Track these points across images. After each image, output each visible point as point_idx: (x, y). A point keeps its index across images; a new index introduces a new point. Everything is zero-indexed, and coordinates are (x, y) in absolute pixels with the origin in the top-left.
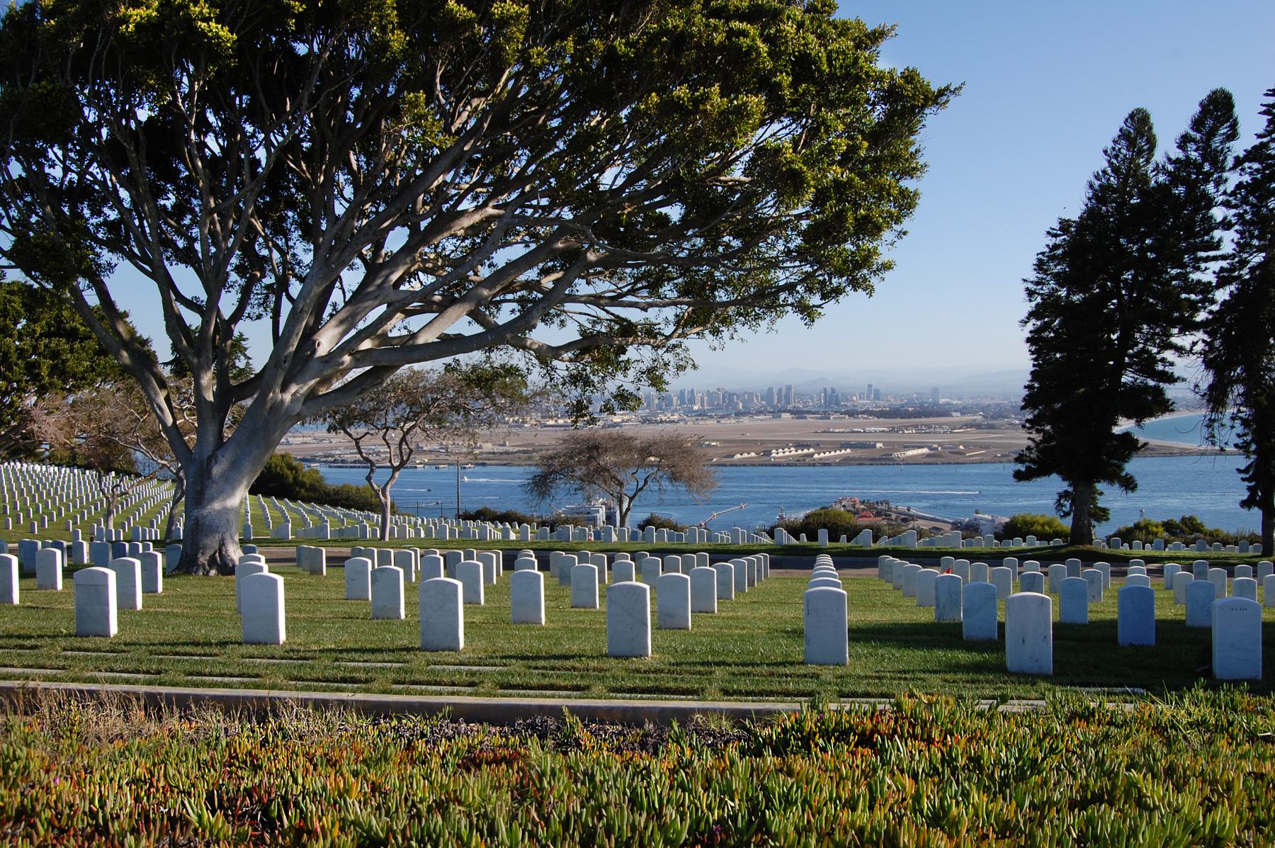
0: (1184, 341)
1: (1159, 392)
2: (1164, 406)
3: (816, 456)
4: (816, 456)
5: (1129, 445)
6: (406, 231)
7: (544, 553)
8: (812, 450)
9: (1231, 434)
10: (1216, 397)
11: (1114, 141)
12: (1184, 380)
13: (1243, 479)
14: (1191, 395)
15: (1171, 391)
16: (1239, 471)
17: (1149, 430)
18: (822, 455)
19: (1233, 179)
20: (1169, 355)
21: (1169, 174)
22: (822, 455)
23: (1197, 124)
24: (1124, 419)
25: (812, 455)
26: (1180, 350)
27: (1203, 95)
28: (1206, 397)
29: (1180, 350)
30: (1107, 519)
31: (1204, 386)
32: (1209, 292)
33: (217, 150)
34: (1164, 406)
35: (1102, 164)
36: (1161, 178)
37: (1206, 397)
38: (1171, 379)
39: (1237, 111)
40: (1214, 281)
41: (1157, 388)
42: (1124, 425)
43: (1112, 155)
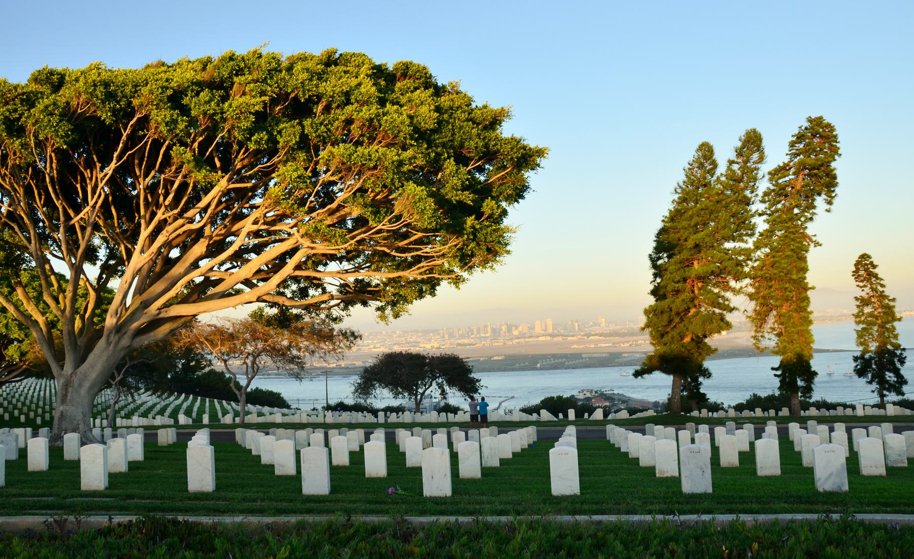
1: (722, 319)
3: (567, 363)
4: (567, 363)
7: (391, 430)
8: (564, 360)
12: (737, 309)
13: (775, 375)
14: (744, 319)
15: (729, 317)
16: (773, 369)
18: (570, 362)
20: (728, 295)
22: (570, 362)
23: (740, 153)
25: (564, 362)
26: (733, 290)
27: (742, 133)
28: (318, 312)
29: (733, 290)
30: (500, 459)
31: (750, 313)
35: (681, 178)
37: (318, 312)
38: (731, 310)
39: (765, 143)
40: (752, 247)
41: (721, 314)
43: (689, 173)
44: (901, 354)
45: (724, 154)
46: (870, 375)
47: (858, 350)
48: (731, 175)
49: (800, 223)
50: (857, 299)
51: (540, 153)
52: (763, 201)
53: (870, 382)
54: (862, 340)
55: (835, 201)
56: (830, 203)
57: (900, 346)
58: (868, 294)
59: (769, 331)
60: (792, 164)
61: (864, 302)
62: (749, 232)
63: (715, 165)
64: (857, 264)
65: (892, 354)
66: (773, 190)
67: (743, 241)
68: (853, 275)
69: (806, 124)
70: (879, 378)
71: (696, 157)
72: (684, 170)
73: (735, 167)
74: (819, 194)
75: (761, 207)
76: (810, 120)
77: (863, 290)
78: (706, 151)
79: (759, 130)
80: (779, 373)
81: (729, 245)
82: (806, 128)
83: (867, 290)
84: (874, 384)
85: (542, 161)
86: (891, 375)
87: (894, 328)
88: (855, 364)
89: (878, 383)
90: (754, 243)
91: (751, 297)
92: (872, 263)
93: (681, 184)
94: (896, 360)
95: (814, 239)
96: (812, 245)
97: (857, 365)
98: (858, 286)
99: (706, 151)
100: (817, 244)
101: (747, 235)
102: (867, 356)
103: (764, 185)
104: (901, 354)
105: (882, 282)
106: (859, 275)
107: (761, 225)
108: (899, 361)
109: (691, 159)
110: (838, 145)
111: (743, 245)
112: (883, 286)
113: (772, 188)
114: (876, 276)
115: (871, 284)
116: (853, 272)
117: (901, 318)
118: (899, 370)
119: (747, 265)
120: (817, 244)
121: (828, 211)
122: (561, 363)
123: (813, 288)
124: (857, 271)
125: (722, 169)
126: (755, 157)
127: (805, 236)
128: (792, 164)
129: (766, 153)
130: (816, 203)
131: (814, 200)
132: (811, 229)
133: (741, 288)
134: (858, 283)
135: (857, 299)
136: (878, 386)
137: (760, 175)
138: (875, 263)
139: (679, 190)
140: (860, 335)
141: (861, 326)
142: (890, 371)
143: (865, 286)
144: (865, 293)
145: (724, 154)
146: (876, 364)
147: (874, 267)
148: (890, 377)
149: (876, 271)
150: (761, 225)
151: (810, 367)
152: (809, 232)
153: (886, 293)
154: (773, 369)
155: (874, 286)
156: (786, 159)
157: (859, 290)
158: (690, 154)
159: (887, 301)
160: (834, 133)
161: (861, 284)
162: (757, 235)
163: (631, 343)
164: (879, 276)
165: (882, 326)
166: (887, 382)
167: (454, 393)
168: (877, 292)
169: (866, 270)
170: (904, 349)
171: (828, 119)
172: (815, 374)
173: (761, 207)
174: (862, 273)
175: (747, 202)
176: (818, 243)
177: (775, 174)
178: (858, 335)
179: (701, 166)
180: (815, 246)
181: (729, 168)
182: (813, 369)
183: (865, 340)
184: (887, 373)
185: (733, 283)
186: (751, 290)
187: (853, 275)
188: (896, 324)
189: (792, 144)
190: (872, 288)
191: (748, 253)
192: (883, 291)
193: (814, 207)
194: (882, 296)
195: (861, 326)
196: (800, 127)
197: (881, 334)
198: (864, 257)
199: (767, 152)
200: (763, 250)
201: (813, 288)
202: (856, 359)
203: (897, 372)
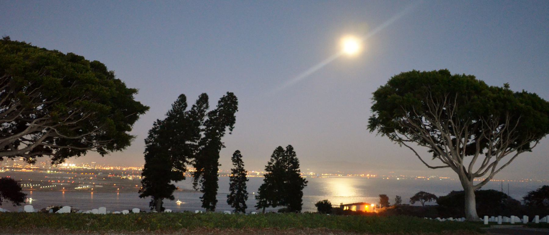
0: (190, 160)
2: (184, 178)
5: (173, 188)
6: (37, 108)
9: (200, 186)
10: (196, 175)
11: (175, 103)
17: (179, 184)
19: (206, 118)
20: (185, 164)
21: (189, 115)
23: (198, 102)
24: (176, 186)
26: (188, 162)
29: (188, 162)
32: (194, 139)
33: (31, 199)
34: (184, 178)
35: (171, 108)
36: (187, 115)
39: (209, 100)
42: (172, 182)
43: (174, 106)
44: (246, 195)
45: (191, 102)
46: (233, 204)
47: (229, 193)
48: (193, 112)
49: (218, 137)
50: (232, 170)
51: (147, 108)
52: (204, 125)
53: (233, 207)
54: (232, 188)
55: (233, 130)
56: (231, 130)
57: (246, 191)
58: (237, 168)
59: (200, 181)
60: (218, 110)
61: (235, 171)
62: (198, 138)
63: (186, 106)
64: (234, 155)
65: (243, 195)
66: (209, 121)
67: (194, 141)
68: (232, 159)
69: (226, 95)
70: (236, 206)
71: (178, 100)
72: (172, 105)
73: (195, 108)
74: (227, 126)
75: (204, 127)
76: (228, 93)
77: (235, 166)
78: (183, 98)
79: (208, 94)
80: (203, 199)
81: (188, 142)
82: (226, 97)
83: (237, 166)
84: (234, 207)
85: (146, 112)
86: (241, 204)
87: (245, 184)
88: (227, 199)
89: (236, 207)
90: (199, 143)
91: (195, 166)
92: (240, 155)
93: (170, 112)
94: (244, 198)
95: (223, 144)
96: (222, 147)
97: (228, 199)
98: (233, 164)
99: (183, 98)
100: (224, 147)
101: (196, 139)
102: (233, 195)
103: (206, 118)
104: (246, 195)
105: (243, 164)
106: (234, 160)
107: (203, 135)
108: (245, 198)
109: (176, 100)
110: (237, 106)
111: (195, 143)
112: (243, 165)
113: (209, 120)
114: (241, 160)
115: (239, 164)
116: (232, 158)
117: (248, 180)
118: (245, 202)
119: (195, 152)
120: (224, 147)
121: (230, 133)
122: (37, 187)
123: (220, 165)
124: (233, 158)
125: (189, 108)
126: (205, 105)
127: (220, 143)
128: (218, 110)
129: (209, 105)
130: (225, 129)
131: (225, 127)
132: (222, 140)
133: (191, 162)
134: (233, 163)
135: (232, 170)
136: (235, 209)
137: (206, 113)
138: (242, 155)
139: (168, 114)
140: (232, 186)
141: (232, 182)
142: (241, 202)
143: (236, 165)
144: (235, 168)
145: (191, 102)
146: (236, 199)
147: (241, 157)
148: (241, 205)
149: (241, 158)
150: (203, 135)
151: (215, 198)
152: (222, 141)
153: (244, 169)
154: (200, 198)
155: (240, 165)
156: (216, 108)
157: (234, 166)
158: (175, 98)
159: (243, 172)
160: (237, 101)
161: (235, 163)
162: (201, 139)
163: (85, 178)
164: (242, 161)
165: (240, 182)
166: (239, 207)
167: (7, 202)
168: (240, 168)
169: (238, 157)
170: (248, 193)
171: (235, 94)
172: (217, 201)
173: (204, 127)
174: (236, 158)
175: (199, 124)
176: (224, 146)
177: (210, 114)
178: (231, 186)
179: (180, 105)
180: (223, 147)
181: (192, 109)
182: (216, 199)
183: (233, 188)
184: (240, 203)
185: (187, 159)
186: (195, 163)
187: (232, 159)
188: (246, 182)
189: (219, 102)
190: (239, 166)
191: (196, 147)
192: (243, 168)
193: (225, 131)
194: (242, 170)
195: (232, 182)
196: (224, 96)
197: (240, 186)
198: (238, 152)
199: (210, 104)
200: (202, 146)
201: (220, 165)
202: (228, 196)
203: (244, 203)
